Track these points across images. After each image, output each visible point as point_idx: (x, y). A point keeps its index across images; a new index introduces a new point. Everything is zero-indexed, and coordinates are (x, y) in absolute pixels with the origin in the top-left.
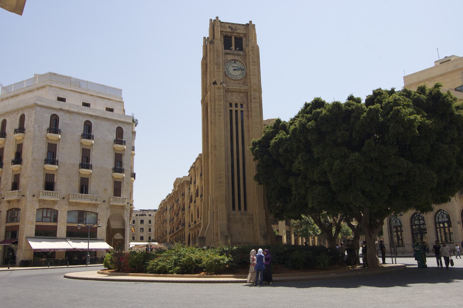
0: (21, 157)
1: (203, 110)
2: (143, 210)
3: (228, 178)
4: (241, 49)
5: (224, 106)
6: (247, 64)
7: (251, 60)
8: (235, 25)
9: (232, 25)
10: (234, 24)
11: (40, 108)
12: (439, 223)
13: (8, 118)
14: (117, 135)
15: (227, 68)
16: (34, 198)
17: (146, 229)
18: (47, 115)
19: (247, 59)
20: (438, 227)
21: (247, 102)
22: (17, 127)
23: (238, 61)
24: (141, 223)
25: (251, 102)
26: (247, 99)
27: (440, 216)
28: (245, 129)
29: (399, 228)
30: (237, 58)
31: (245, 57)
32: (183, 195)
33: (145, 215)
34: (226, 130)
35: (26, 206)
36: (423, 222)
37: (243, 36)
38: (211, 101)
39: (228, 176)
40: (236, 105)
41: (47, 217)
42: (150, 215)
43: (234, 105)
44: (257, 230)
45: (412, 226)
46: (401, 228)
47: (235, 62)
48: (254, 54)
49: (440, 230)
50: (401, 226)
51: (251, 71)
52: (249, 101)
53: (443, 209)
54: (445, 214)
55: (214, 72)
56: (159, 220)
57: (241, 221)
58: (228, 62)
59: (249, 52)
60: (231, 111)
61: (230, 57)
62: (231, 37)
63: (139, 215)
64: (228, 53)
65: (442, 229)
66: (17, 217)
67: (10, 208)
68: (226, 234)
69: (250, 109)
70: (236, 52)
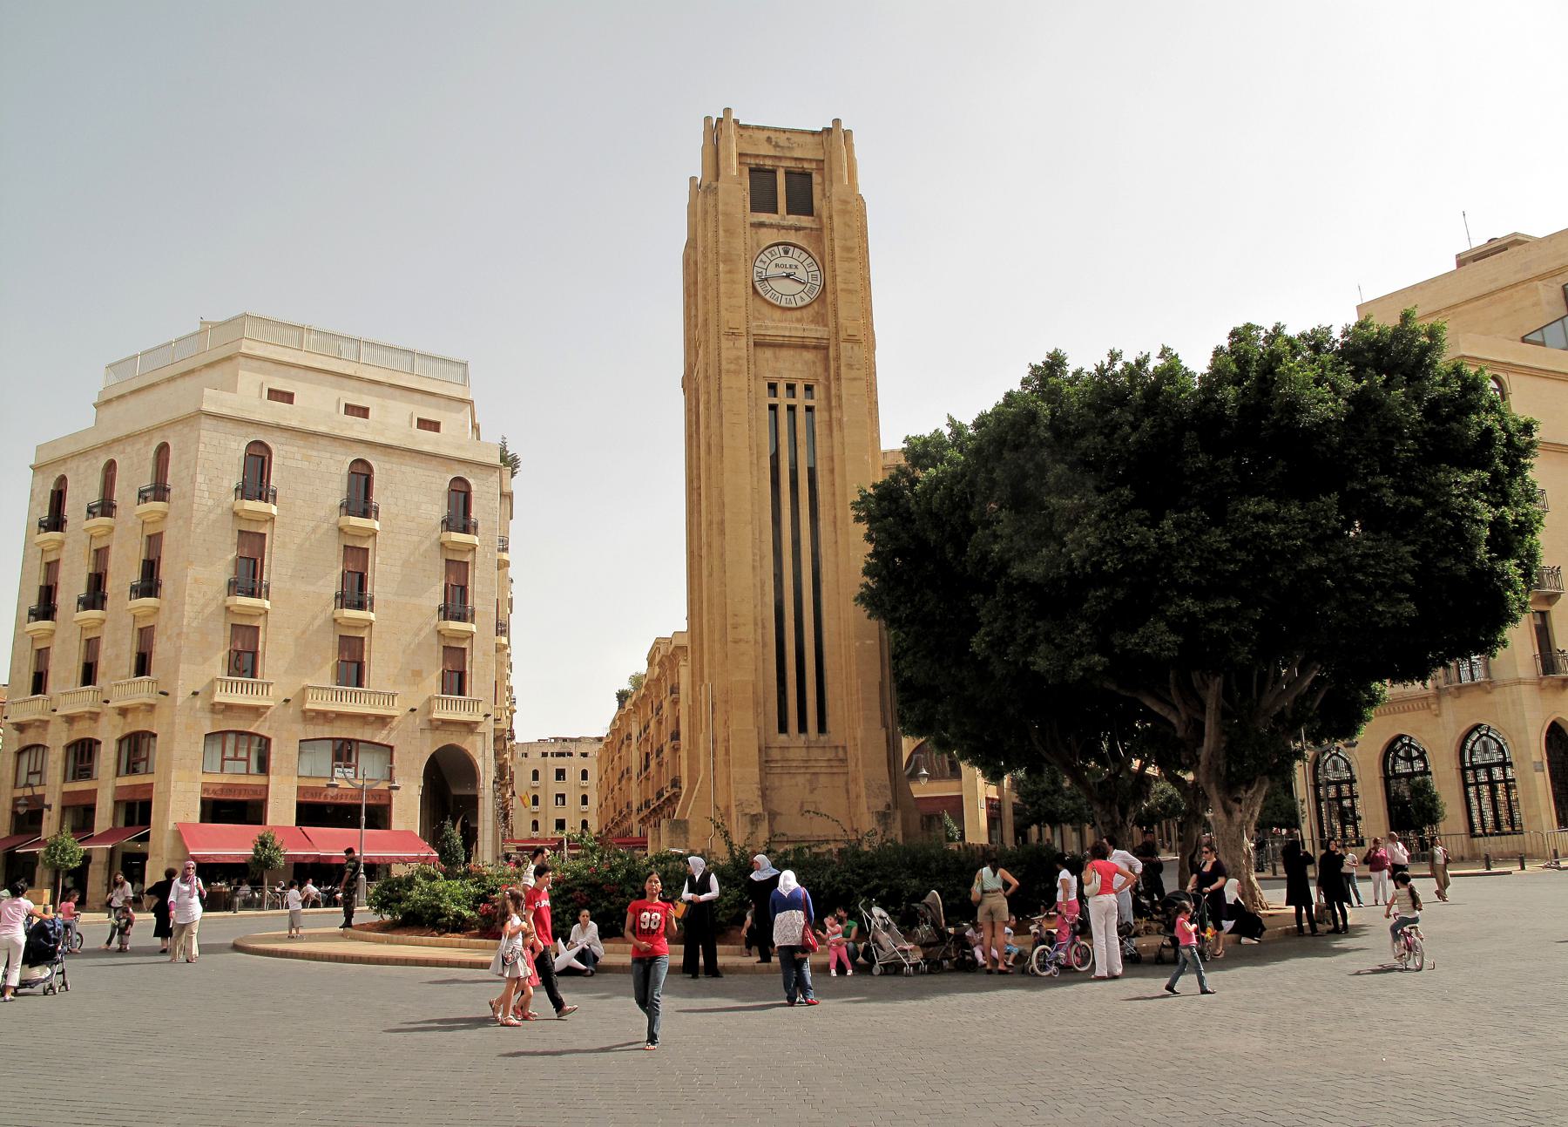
0: (157, 578)
1: (688, 410)
2: (565, 740)
3: (764, 627)
4: (755, 172)
5: (749, 391)
6: (827, 256)
7: (837, 243)
9: (778, 134)
11: (215, 422)
12: (1475, 768)
13: (122, 456)
15: (760, 270)
16: (198, 703)
17: (573, 799)
18: (234, 445)
19: (827, 242)
20: (1471, 780)
21: (828, 379)
22: (147, 482)
23: (795, 246)
24: (558, 778)
25: (838, 378)
26: (827, 369)
27: (1478, 747)
28: (825, 550)
29: (1345, 788)
30: (792, 237)
31: (817, 234)
32: (674, 690)
33: (570, 754)
34: (755, 473)
35: (173, 724)
36: (1422, 765)
38: (707, 377)
39: (762, 620)
41: (235, 759)
42: (584, 755)
43: (782, 389)
44: (858, 797)
45: (1387, 780)
46: (1351, 788)
47: (786, 252)
48: (849, 226)
49: (1478, 790)
50: (1351, 781)
51: (838, 279)
52: (832, 377)
53: (1486, 723)
54: (1495, 740)
55: (718, 284)
56: (609, 770)
57: (807, 767)
58: (763, 252)
59: (831, 217)
61: (769, 237)
63: (552, 755)
64: (761, 225)
65: (1485, 790)
66: (146, 759)
67: (128, 731)
68: (758, 809)
70: (793, 220)
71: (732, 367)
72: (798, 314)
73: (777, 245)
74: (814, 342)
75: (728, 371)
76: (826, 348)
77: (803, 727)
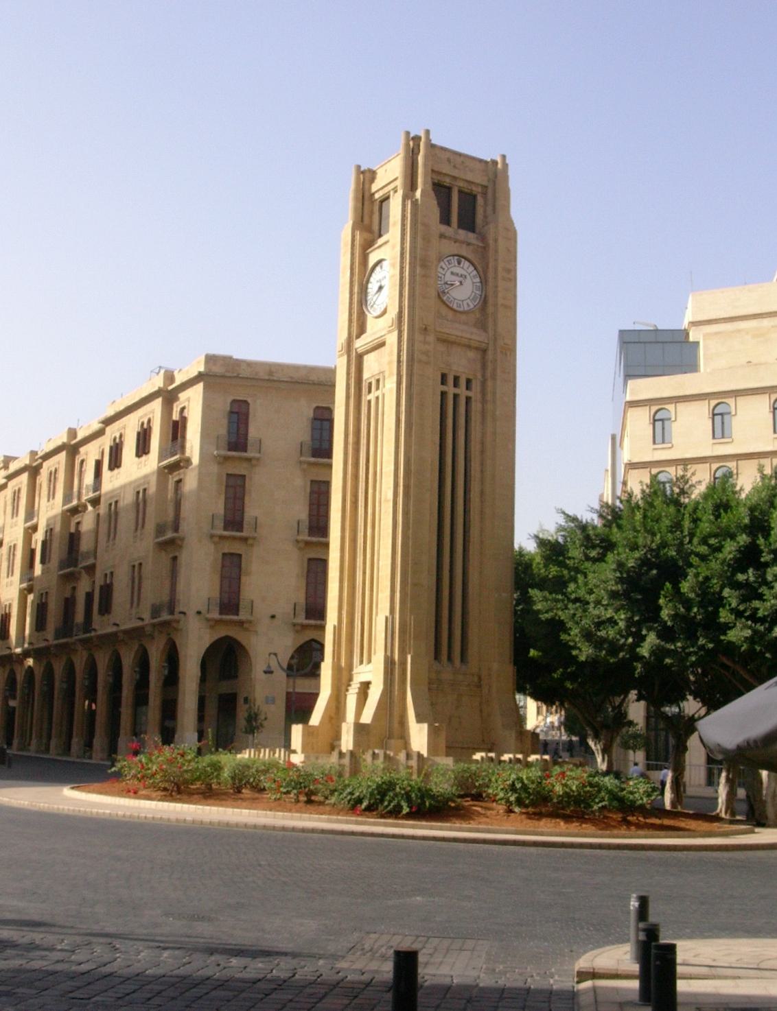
8: (462, 159)
10: (460, 155)
14: (346, 584)
25: (494, 377)
28: (475, 448)
37: (479, 192)
40: (456, 379)
47: (459, 263)
60: (443, 394)
62: (449, 189)
69: (489, 397)
71: (424, 358)
72: (463, 317)
73: (454, 256)
74: (477, 344)
75: (420, 361)
76: (484, 351)
77: (450, 658)
